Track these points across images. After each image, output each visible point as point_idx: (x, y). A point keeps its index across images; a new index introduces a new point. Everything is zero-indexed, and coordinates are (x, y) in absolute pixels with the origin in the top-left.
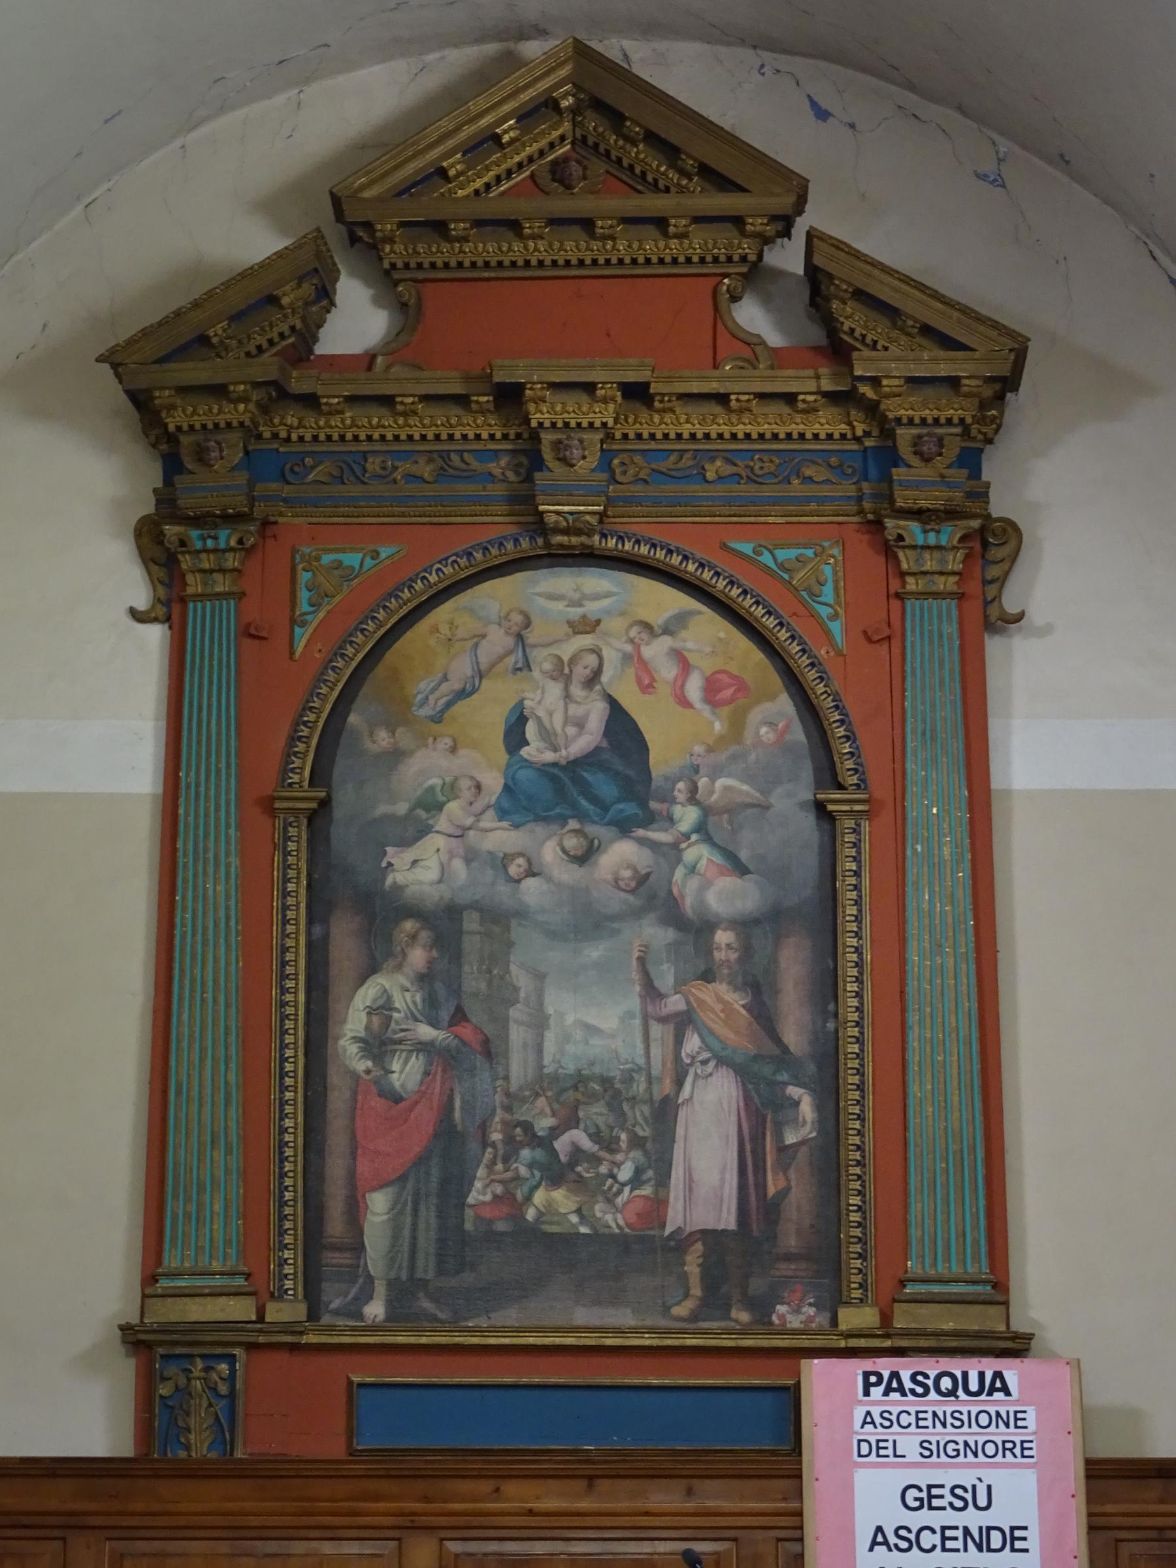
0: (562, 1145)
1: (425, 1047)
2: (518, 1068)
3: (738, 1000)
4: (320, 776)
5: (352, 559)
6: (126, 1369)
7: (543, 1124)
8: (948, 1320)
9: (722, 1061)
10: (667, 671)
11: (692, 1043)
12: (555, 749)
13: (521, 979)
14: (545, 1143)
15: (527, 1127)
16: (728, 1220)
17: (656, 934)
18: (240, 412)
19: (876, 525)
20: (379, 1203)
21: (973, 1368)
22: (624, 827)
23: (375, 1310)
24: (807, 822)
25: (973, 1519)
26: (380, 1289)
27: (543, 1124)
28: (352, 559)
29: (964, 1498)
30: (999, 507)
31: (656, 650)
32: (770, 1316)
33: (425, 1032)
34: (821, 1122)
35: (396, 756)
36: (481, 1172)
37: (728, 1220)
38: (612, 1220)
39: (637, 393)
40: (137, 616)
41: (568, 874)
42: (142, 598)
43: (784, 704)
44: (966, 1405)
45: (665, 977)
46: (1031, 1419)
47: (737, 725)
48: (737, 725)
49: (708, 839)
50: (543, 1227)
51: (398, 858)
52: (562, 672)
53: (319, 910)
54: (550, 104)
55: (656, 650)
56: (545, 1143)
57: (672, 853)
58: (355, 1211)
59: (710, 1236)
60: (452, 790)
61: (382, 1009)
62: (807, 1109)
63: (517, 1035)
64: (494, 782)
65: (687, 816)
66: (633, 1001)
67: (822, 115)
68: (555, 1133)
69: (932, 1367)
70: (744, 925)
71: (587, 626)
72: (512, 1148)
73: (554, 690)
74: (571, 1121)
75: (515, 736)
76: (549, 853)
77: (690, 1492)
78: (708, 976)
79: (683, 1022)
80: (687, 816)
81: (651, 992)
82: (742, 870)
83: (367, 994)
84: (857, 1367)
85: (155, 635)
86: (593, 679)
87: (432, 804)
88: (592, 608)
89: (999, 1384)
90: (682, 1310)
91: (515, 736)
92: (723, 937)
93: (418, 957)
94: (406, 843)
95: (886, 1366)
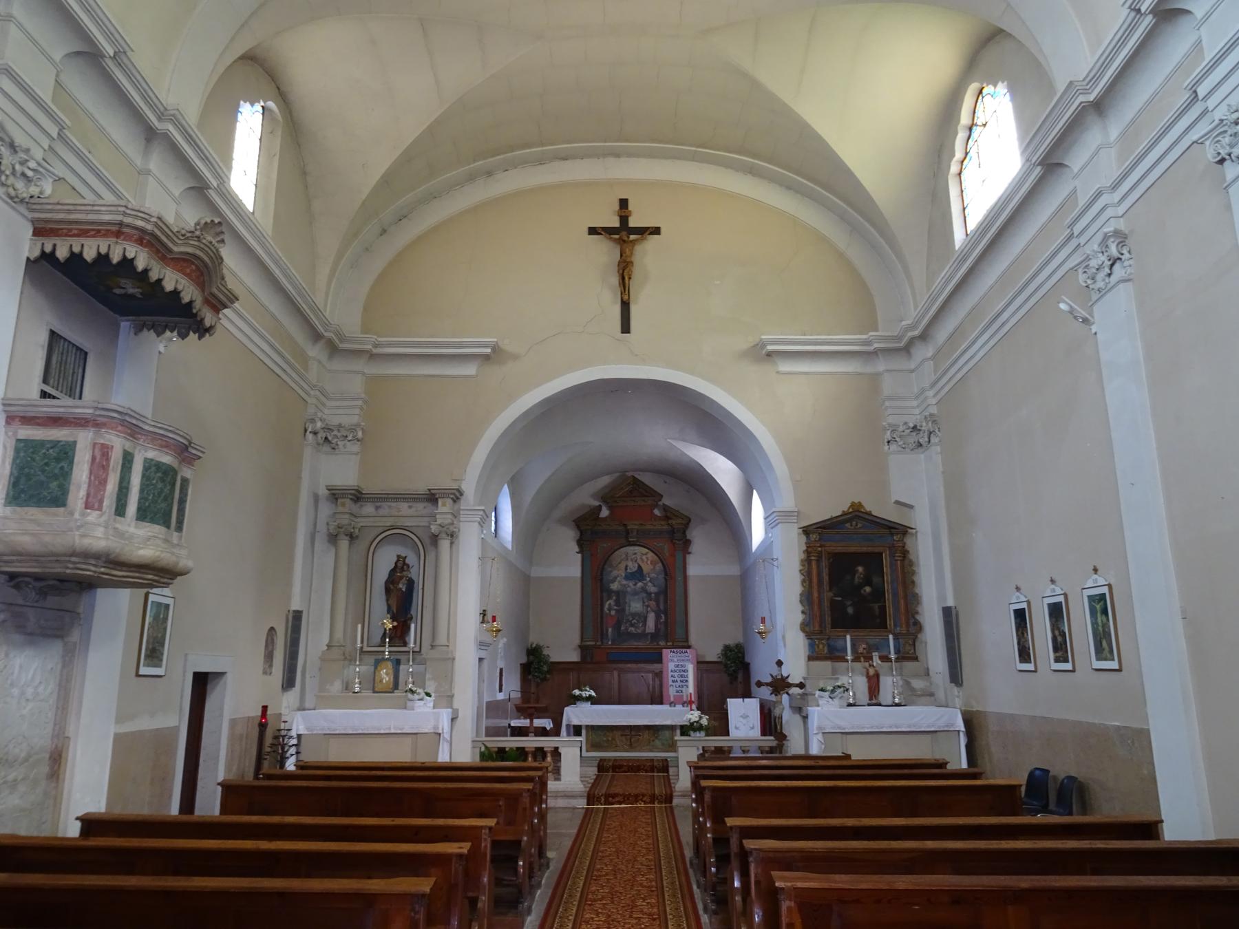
1: (615, 610)
2: (627, 612)
3: (654, 603)
4: (602, 574)
5: (605, 545)
6: (579, 650)
8: (681, 644)
9: (653, 611)
10: (646, 560)
11: (649, 609)
13: (627, 601)
14: (631, 621)
16: (653, 631)
17: (644, 595)
18: (589, 527)
19: (672, 541)
20: (610, 630)
21: (684, 650)
22: (640, 581)
23: (610, 643)
24: (663, 580)
25: (683, 669)
27: (631, 619)
28: (605, 545)
29: (682, 666)
30: (688, 537)
31: (644, 557)
32: (775, 737)
33: (615, 608)
34: (665, 619)
35: (611, 572)
37: (653, 631)
38: (639, 631)
39: (641, 524)
40: (577, 553)
41: (633, 587)
42: (578, 550)
43: (660, 564)
44: (682, 655)
45: (645, 600)
46: (690, 656)
47: (654, 568)
48: (654, 568)
49: (651, 582)
50: (509, 546)
51: (611, 585)
52: (632, 560)
53: (602, 591)
54: (630, 483)
55: (644, 557)
56: (631, 621)
57: (646, 584)
58: (607, 631)
59: (651, 633)
60: (618, 576)
61: (610, 604)
62: (663, 617)
63: (627, 608)
64: (624, 575)
65: (648, 579)
66: (642, 604)
67: (666, 482)
69: (678, 650)
70: (656, 594)
71: (635, 554)
72: (626, 623)
73: (631, 563)
74: (634, 619)
75: (626, 569)
76: (631, 584)
77: (377, 508)
78: (651, 600)
79: (648, 606)
80: (648, 579)
81: (644, 602)
82: (655, 586)
83: (608, 603)
84: (669, 650)
85: (580, 555)
86: (636, 561)
87: (616, 578)
88: (636, 551)
89: (687, 652)
90: (648, 643)
91: (626, 569)
92: (653, 595)
93: (614, 598)
94: (613, 583)
95: (672, 650)
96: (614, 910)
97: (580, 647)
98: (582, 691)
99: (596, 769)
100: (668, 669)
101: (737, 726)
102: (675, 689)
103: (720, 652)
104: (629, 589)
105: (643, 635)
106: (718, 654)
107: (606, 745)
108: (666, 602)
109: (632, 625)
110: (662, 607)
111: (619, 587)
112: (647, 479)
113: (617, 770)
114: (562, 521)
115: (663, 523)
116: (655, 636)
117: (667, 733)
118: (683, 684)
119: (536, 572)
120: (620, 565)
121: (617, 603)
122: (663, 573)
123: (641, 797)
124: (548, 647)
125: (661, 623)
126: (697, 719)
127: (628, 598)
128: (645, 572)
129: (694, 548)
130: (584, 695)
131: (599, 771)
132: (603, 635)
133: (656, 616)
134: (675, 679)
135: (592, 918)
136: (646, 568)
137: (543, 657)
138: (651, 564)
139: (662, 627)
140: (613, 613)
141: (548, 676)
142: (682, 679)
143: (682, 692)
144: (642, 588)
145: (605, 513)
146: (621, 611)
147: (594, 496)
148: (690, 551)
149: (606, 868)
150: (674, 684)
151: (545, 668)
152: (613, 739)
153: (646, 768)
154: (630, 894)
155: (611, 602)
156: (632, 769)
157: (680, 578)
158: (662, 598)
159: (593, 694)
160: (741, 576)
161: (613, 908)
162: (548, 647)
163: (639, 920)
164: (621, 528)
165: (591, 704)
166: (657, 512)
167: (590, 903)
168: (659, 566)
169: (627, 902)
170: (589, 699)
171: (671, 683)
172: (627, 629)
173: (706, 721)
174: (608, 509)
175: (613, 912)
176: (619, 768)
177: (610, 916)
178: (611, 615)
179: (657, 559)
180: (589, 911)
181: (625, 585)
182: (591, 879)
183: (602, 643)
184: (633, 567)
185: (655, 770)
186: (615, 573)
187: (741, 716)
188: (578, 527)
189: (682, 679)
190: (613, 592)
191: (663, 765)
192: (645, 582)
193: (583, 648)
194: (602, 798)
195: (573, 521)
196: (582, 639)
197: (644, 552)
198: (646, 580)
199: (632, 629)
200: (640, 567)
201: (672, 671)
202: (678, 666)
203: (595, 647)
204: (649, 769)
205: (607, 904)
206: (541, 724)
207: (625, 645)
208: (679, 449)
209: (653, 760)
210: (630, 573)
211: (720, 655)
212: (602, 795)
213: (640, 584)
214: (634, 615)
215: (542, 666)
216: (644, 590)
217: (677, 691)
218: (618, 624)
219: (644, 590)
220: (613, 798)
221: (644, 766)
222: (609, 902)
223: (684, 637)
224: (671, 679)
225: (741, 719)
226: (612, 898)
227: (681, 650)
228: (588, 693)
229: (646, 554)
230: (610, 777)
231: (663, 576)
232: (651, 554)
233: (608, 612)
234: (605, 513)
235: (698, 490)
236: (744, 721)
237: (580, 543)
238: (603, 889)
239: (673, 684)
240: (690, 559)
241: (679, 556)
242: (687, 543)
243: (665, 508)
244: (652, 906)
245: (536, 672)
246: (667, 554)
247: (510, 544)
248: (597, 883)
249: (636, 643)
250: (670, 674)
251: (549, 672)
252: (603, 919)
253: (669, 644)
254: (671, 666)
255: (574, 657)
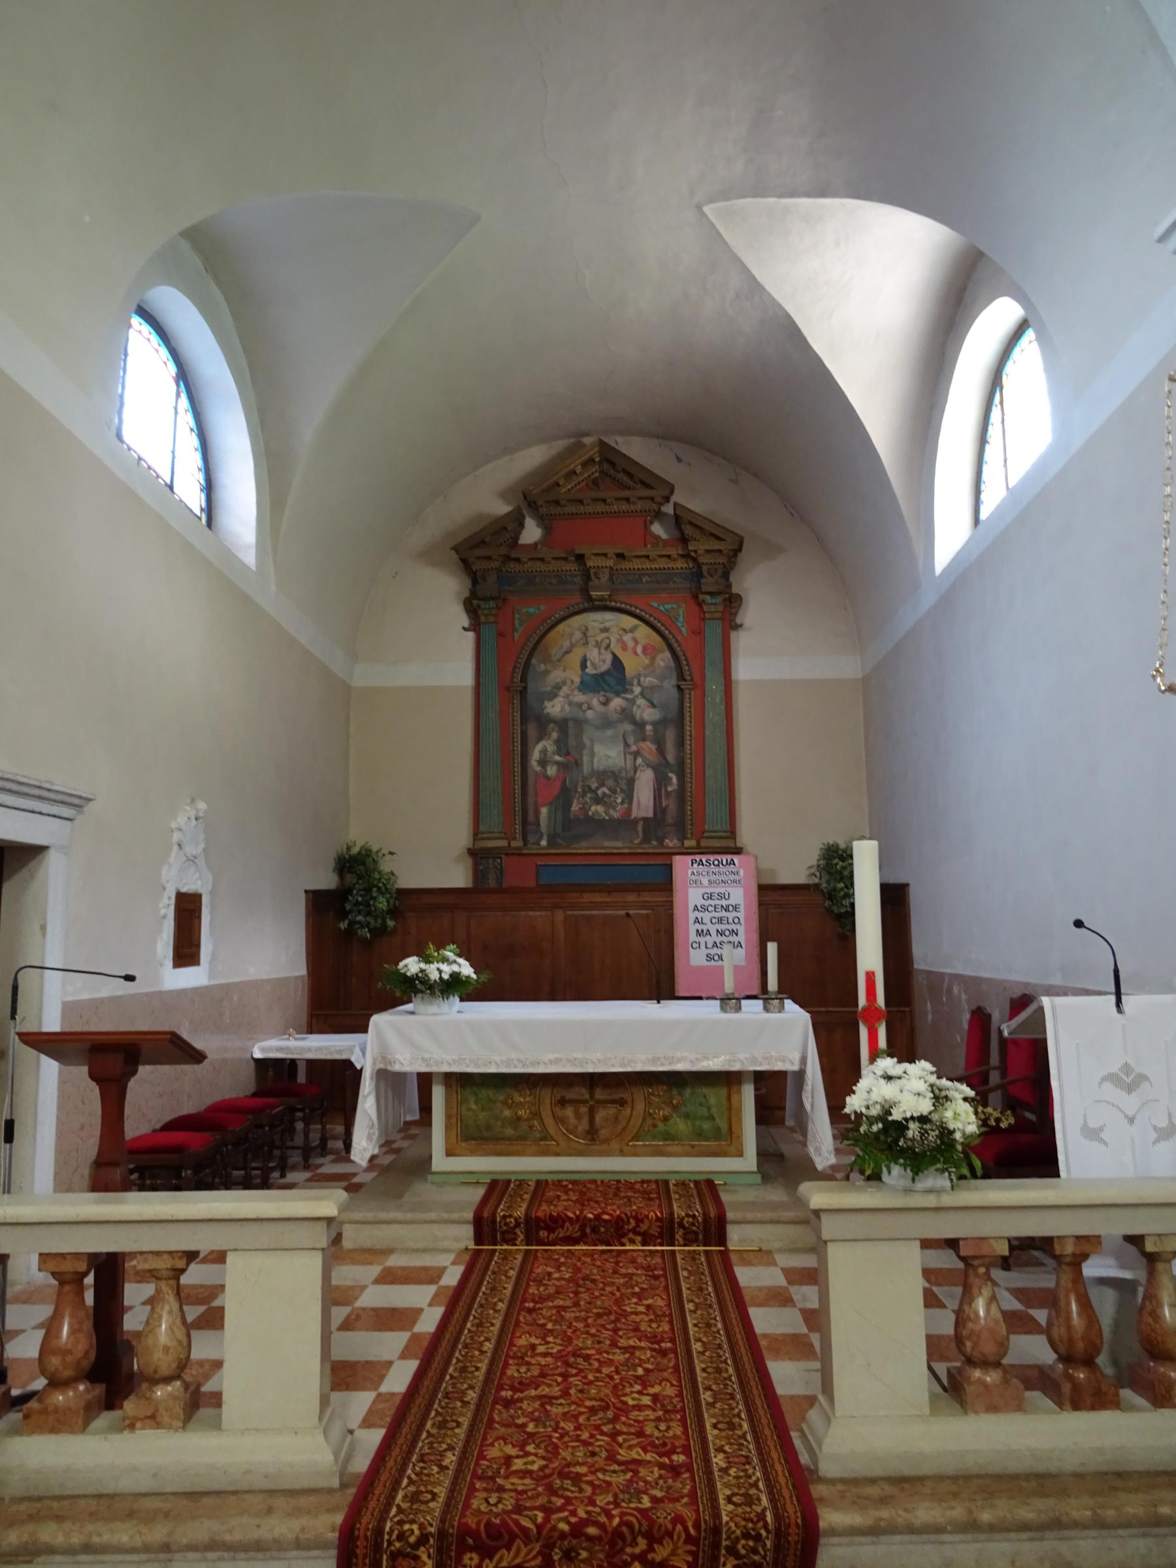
0: (600, 792)
1: (557, 763)
2: (586, 769)
3: (653, 747)
4: (523, 679)
5: (532, 610)
6: (469, 862)
7: (594, 785)
8: (717, 844)
9: (649, 766)
10: (631, 644)
12: (596, 669)
13: (586, 741)
14: (595, 792)
15: (589, 787)
16: (650, 814)
17: (628, 727)
18: (495, 564)
19: (695, 597)
20: (544, 811)
21: (725, 858)
22: (618, 694)
23: (544, 843)
25: (724, 903)
26: (545, 837)
28: (532, 610)
29: (721, 896)
30: (735, 590)
31: (627, 638)
33: (558, 758)
35: (547, 672)
36: (575, 801)
37: (650, 814)
38: (615, 815)
40: (464, 629)
42: (466, 624)
44: (722, 869)
45: (631, 740)
46: (742, 872)
50: (250, 558)
52: (598, 645)
53: (524, 720)
55: (627, 638)
60: (564, 683)
61: (544, 751)
62: (674, 780)
64: (577, 680)
65: (637, 690)
66: (621, 747)
68: (598, 788)
69: (712, 857)
70: (655, 724)
71: (606, 630)
72: (584, 795)
73: (596, 651)
74: (602, 785)
76: (595, 702)
78: (644, 740)
79: (636, 754)
80: (637, 690)
81: (627, 745)
82: (653, 706)
83: (539, 747)
84: (689, 858)
85: (471, 635)
86: (608, 647)
87: (558, 687)
88: (607, 624)
90: (637, 841)
93: (555, 735)
94: (550, 699)
95: (698, 858)
96: (580, 1325)
97: (473, 853)
98: (428, 961)
99: (467, 1231)
100: (687, 907)
101: (1093, 1124)
102: (703, 952)
103: (814, 862)
104: (590, 714)
105: (626, 823)
106: (811, 867)
107: (509, 1132)
108: (680, 743)
109: (598, 801)
110: (671, 757)
111: (567, 707)
112: (636, 449)
113: (543, 1234)
114: (428, 555)
115: (673, 552)
116: (654, 826)
117: (714, 1096)
118: (724, 939)
119: (365, 676)
120: (568, 656)
121: (562, 746)
122: (675, 676)
123: (642, 1543)
124: (391, 853)
125: (668, 794)
126: (925, 1106)
127: (588, 734)
128: (629, 672)
129: (750, 615)
130: (434, 976)
131: (479, 1239)
132: (528, 825)
133: (656, 777)
134: (705, 928)
135: (550, 1274)
136: (631, 664)
137: (377, 876)
138: (645, 651)
139: (671, 805)
140: (551, 771)
141: (391, 923)
142: (720, 927)
143: (721, 958)
144: (623, 710)
145: (532, 533)
146: (572, 764)
147: (505, 495)
148: (738, 621)
149: (556, 1275)
150: (702, 940)
151: (382, 903)
152: (536, 1115)
153: (644, 1227)
154: (613, 1284)
155: (548, 744)
156: (595, 1230)
157: (714, 686)
158: (670, 736)
159: (466, 969)
160: (866, 679)
161: (577, 1319)
162: (391, 853)
163: (632, 1354)
164: (572, 566)
165: (462, 1000)
166: (657, 529)
167: (531, 1305)
168: (664, 659)
169: (606, 1305)
170: (453, 986)
171: (693, 936)
172: (584, 809)
173: (967, 1108)
174: (538, 526)
175: (584, 1263)
176: (551, 1230)
177: (570, 1340)
178: (548, 778)
179: (659, 639)
180: (527, 1328)
181: (580, 705)
182: (521, 1309)
183: (525, 843)
184: (600, 662)
185: (678, 1236)
186: (556, 675)
187: (1112, 1078)
188: (466, 564)
189: (720, 927)
190: (554, 721)
191: (706, 1215)
192: (629, 696)
193: (477, 855)
194: (518, 1231)
195: (452, 549)
196: (476, 834)
197: (627, 627)
198: (632, 691)
199: (598, 810)
200: (616, 662)
201: (696, 908)
202: (711, 897)
203: (509, 853)
204: (654, 1231)
205: (564, 1308)
206: (340, 1052)
207: (583, 847)
208: (738, 261)
209: (666, 1182)
210: (593, 676)
211: (813, 870)
212: (423, 1540)
213: (617, 702)
214: (603, 776)
215: (374, 899)
216: (627, 715)
217: (710, 958)
218: (565, 796)
219: (627, 715)
220: (551, 1230)
221: (639, 1221)
222: (568, 1303)
223: (727, 827)
224: (693, 928)
225: (1111, 1092)
226: (576, 1293)
227: (719, 857)
228: (447, 969)
229: (633, 630)
230: (520, 1257)
231: (674, 681)
232: (644, 631)
233: (538, 769)
234: (532, 533)
235: (756, 475)
236: (1131, 1102)
237: (471, 606)
238: (560, 1271)
239: (698, 939)
240: (741, 642)
241: (713, 630)
242: (733, 602)
243: (681, 521)
244: (657, 1316)
245: (359, 912)
246: (684, 630)
247: (253, 551)
248: (534, 1323)
249: (607, 844)
250: (692, 916)
251: (393, 912)
252: (567, 1276)
253: (687, 843)
254: (695, 896)
255: (458, 877)
